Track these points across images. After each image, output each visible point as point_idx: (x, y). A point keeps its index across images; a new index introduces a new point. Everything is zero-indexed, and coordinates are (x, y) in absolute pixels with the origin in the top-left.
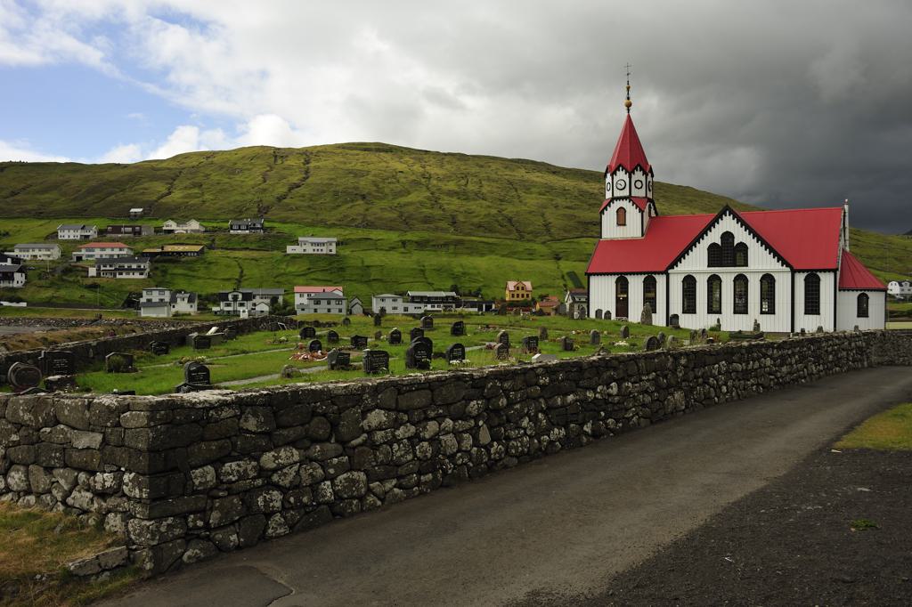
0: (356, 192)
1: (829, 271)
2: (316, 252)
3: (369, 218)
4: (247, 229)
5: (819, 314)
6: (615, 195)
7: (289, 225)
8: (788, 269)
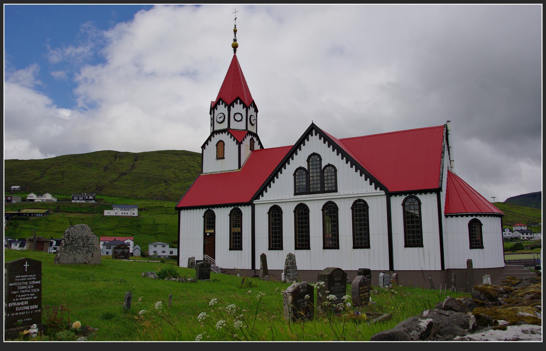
0: (160, 178)
1: (431, 191)
2: (124, 215)
3: (166, 194)
4: (83, 200)
5: (421, 245)
6: (215, 129)
7: (113, 198)
8: (383, 193)
